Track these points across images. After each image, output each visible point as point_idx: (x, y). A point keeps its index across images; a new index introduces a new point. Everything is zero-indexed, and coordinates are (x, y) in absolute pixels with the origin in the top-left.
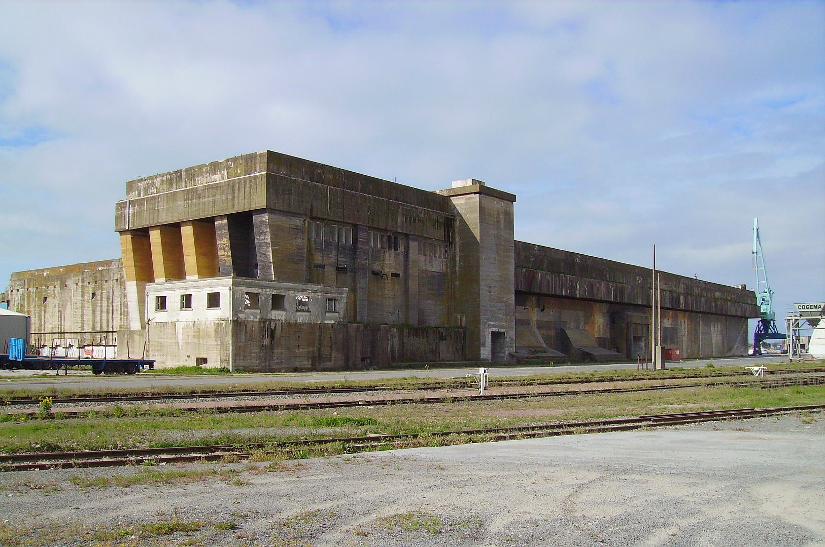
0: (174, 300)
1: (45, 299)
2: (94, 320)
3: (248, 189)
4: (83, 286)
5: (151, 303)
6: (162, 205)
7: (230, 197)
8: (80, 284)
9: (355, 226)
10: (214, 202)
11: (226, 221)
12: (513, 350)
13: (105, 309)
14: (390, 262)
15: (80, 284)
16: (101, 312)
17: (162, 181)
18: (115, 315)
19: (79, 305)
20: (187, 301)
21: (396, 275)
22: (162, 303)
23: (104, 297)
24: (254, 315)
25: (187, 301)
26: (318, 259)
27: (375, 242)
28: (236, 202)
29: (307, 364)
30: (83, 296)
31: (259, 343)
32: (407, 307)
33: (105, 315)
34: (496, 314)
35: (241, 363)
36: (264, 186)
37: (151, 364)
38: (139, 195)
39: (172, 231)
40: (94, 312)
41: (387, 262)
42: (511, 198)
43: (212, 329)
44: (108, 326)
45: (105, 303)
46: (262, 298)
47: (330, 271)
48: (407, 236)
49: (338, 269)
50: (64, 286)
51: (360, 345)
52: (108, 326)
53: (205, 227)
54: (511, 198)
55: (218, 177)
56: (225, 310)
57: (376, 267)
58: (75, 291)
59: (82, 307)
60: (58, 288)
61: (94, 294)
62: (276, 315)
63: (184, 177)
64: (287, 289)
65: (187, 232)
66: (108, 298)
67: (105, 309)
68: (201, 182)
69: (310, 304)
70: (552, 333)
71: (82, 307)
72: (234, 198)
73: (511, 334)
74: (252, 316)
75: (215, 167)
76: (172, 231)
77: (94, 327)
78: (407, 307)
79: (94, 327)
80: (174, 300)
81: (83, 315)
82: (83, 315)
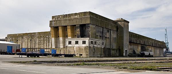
0: (73, 42)
1: (17, 41)
2: (31, 46)
3: (85, 19)
4: (28, 38)
5: (67, 43)
6: (63, 22)
7: (80, 21)
8: (27, 38)
9: (103, 27)
10: (76, 22)
11: (79, 26)
12: (128, 54)
13: (34, 43)
14: (108, 35)
15: (27, 38)
16: (33, 44)
17: (62, 16)
18: (37, 45)
19: (27, 42)
20: (77, 43)
21: (109, 38)
22: (70, 43)
23: (34, 41)
24: (92, 46)
25: (77, 43)
26: (97, 35)
27: (105, 31)
28: (82, 22)
29: (99, 56)
30: (28, 40)
31: (92, 51)
32: (110, 44)
33: (34, 45)
34: (127, 48)
35: (90, 55)
36: (89, 19)
37: (75, 55)
38: (56, 19)
39: (65, 28)
40: (31, 44)
41: (107, 35)
42: (129, 22)
43: (84, 48)
44: (35, 47)
45: (34, 42)
46: (93, 42)
47: (99, 37)
48: (110, 30)
49: (100, 36)
50: (22, 38)
51: (107, 52)
52: (35, 47)
53: (73, 27)
54: (129, 22)
55: (77, 16)
56: (87, 44)
57: (106, 36)
58: (25, 39)
59: (28, 43)
60: (21, 38)
61: (31, 40)
62: (95, 46)
63: (68, 16)
64: (97, 40)
65: (69, 27)
66: (35, 41)
67: (34, 43)
68: (72, 17)
69: (100, 44)
70: (132, 50)
71: (28, 43)
72: (81, 21)
73: (128, 51)
74: (92, 46)
75: (76, 14)
76: (65, 28)
77: (31, 47)
78: (110, 44)
79: (31, 47)
80: (73, 42)
81: (28, 45)
82: (28, 45)
